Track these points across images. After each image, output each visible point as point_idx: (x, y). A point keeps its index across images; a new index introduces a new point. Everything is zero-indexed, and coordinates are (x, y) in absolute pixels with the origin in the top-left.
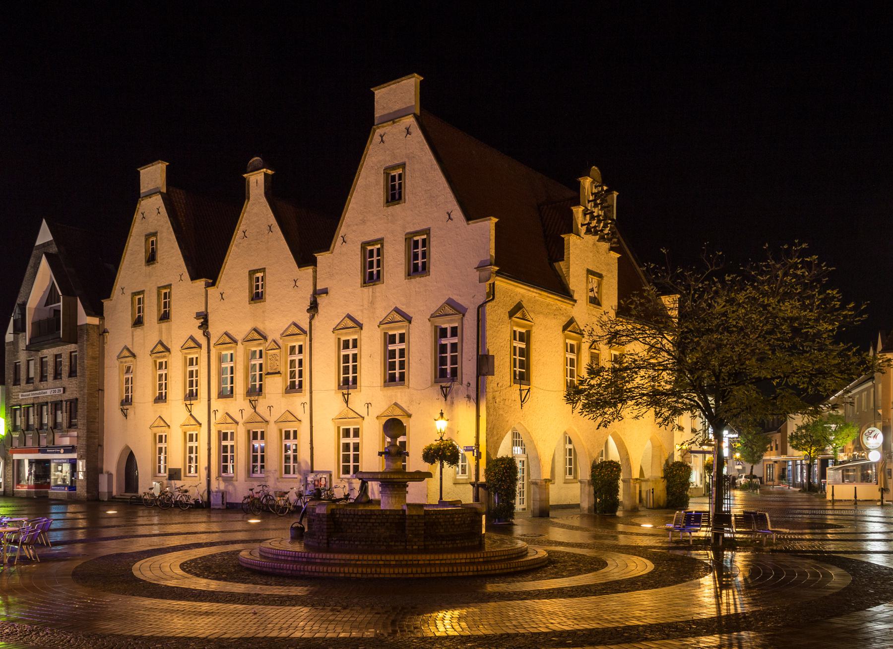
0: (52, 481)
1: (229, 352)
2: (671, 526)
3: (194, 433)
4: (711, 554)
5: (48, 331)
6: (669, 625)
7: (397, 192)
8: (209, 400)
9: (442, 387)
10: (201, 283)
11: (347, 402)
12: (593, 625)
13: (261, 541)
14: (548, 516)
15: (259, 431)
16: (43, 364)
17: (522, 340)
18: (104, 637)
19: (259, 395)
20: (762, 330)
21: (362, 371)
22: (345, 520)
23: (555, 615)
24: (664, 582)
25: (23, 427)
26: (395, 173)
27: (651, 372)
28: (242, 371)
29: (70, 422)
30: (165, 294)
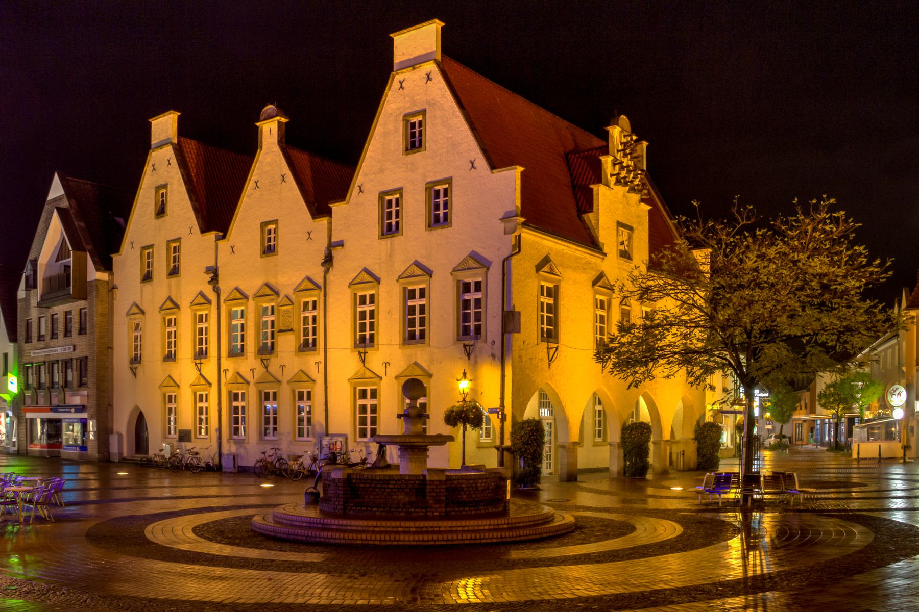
0: (64, 441)
1: (239, 309)
2: (701, 488)
3: (204, 393)
4: (740, 516)
5: (62, 286)
6: (696, 588)
7: (417, 139)
8: (219, 359)
9: (465, 346)
10: (212, 235)
11: (363, 361)
12: (620, 590)
13: (275, 506)
14: (576, 480)
15: (271, 391)
16: (53, 321)
17: (549, 295)
18: (119, 598)
19: (271, 354)
20: (793, 287)
21: (380, 316)
22: (362, 485)
23: (581, 580)
24: (693, 545)
25: (35, 385)
26: (416, 120)
27: (683, 330)
28: (253, 328)
29: (81, 380)
30: (175, 248)
